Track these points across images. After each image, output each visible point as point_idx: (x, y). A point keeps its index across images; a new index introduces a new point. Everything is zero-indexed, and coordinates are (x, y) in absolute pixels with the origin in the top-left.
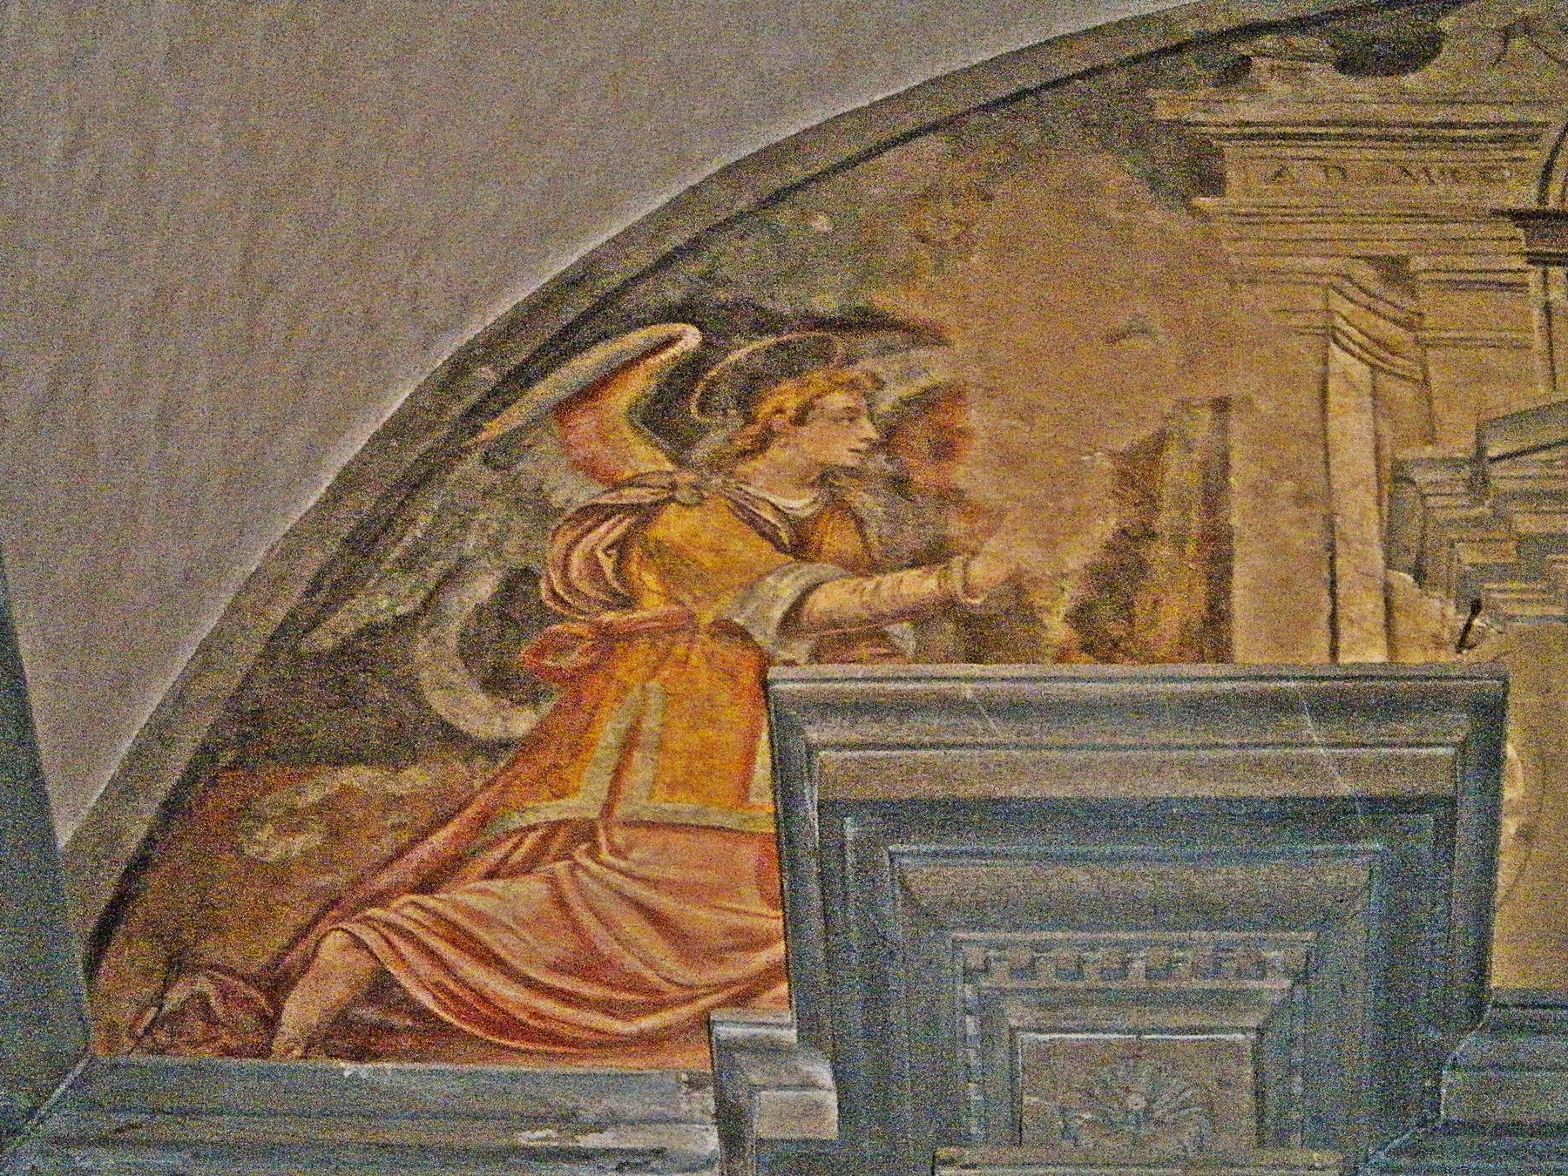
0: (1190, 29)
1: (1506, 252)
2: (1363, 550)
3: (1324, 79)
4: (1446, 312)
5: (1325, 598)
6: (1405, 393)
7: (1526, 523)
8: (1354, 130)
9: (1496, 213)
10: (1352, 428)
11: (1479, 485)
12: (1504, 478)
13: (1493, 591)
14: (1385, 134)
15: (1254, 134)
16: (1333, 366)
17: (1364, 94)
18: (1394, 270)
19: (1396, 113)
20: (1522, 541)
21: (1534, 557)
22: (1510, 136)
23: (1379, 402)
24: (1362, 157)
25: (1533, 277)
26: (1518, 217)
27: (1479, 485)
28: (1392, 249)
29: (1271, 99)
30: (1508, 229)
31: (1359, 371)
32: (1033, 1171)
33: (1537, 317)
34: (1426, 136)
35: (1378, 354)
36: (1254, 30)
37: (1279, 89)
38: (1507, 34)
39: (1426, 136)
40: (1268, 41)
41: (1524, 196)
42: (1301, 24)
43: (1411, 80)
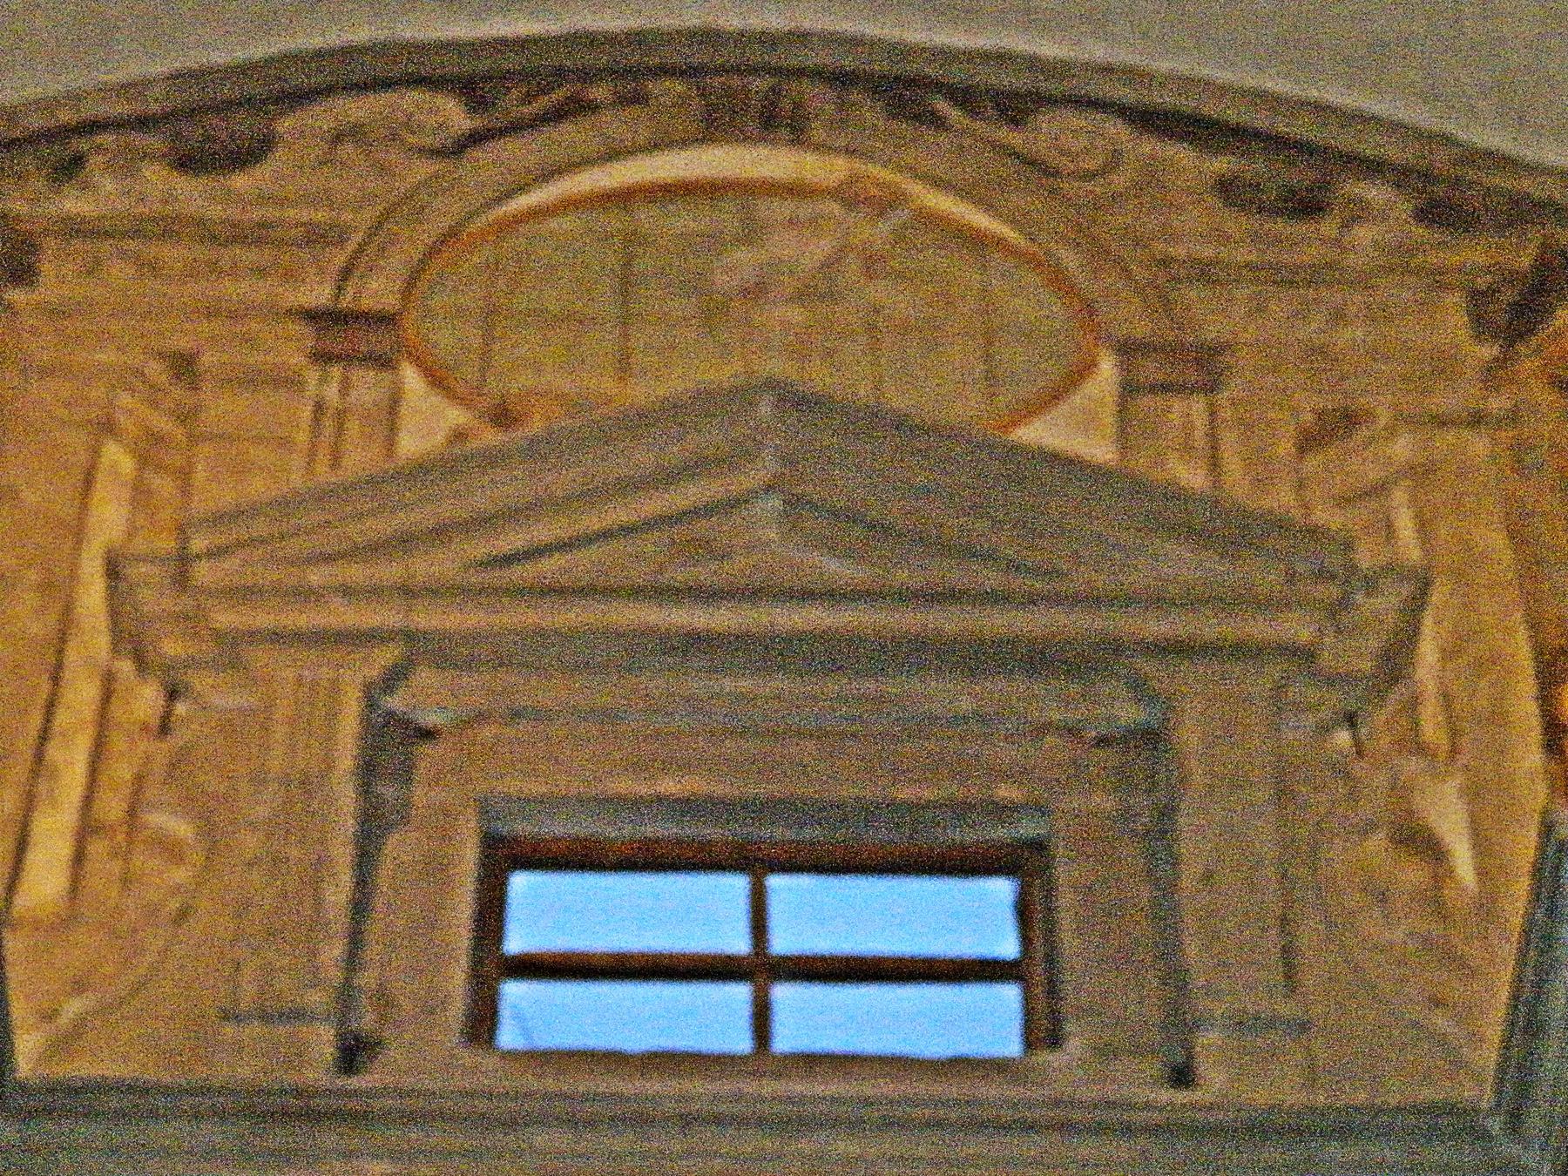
0: (36, 122)
1: (291, 348)
2: (94, 637)
3: (156, 178)
4: (220, 407)
5: (46, 687)
6: (164, 485)
7: (225, 618)
8: (169, 228)
9: (289, 312)
10: (110, 517)
11: (181, 580)
12: (203, 573)
13: (201, 682)
14: (207, 232)
15: (74, 229)
16: (105, 461)
17: (192, 194)
18: (184, 366)
19: (215, 212)
20: (218, 635)
21: (231, 651)
22: (316, 237)
23: (140, 494)
24: (173, 255)
25: (312, 376)
26: (311, 315)
27: (181, 580)
28: (183, 343)
29: (99, 195)
30: (296, 328)
31: (127, 464)
32: (1086, 1148)
33: (307, 413)
34: (238, 235)
35: (149, 450)
36: (93, 126)
37: (109, 185)
38: (338, 138)
39: (238, 235)
40: (107, 139)
41: (319, 294)
42: (143, 123)
43: (240, 181)
